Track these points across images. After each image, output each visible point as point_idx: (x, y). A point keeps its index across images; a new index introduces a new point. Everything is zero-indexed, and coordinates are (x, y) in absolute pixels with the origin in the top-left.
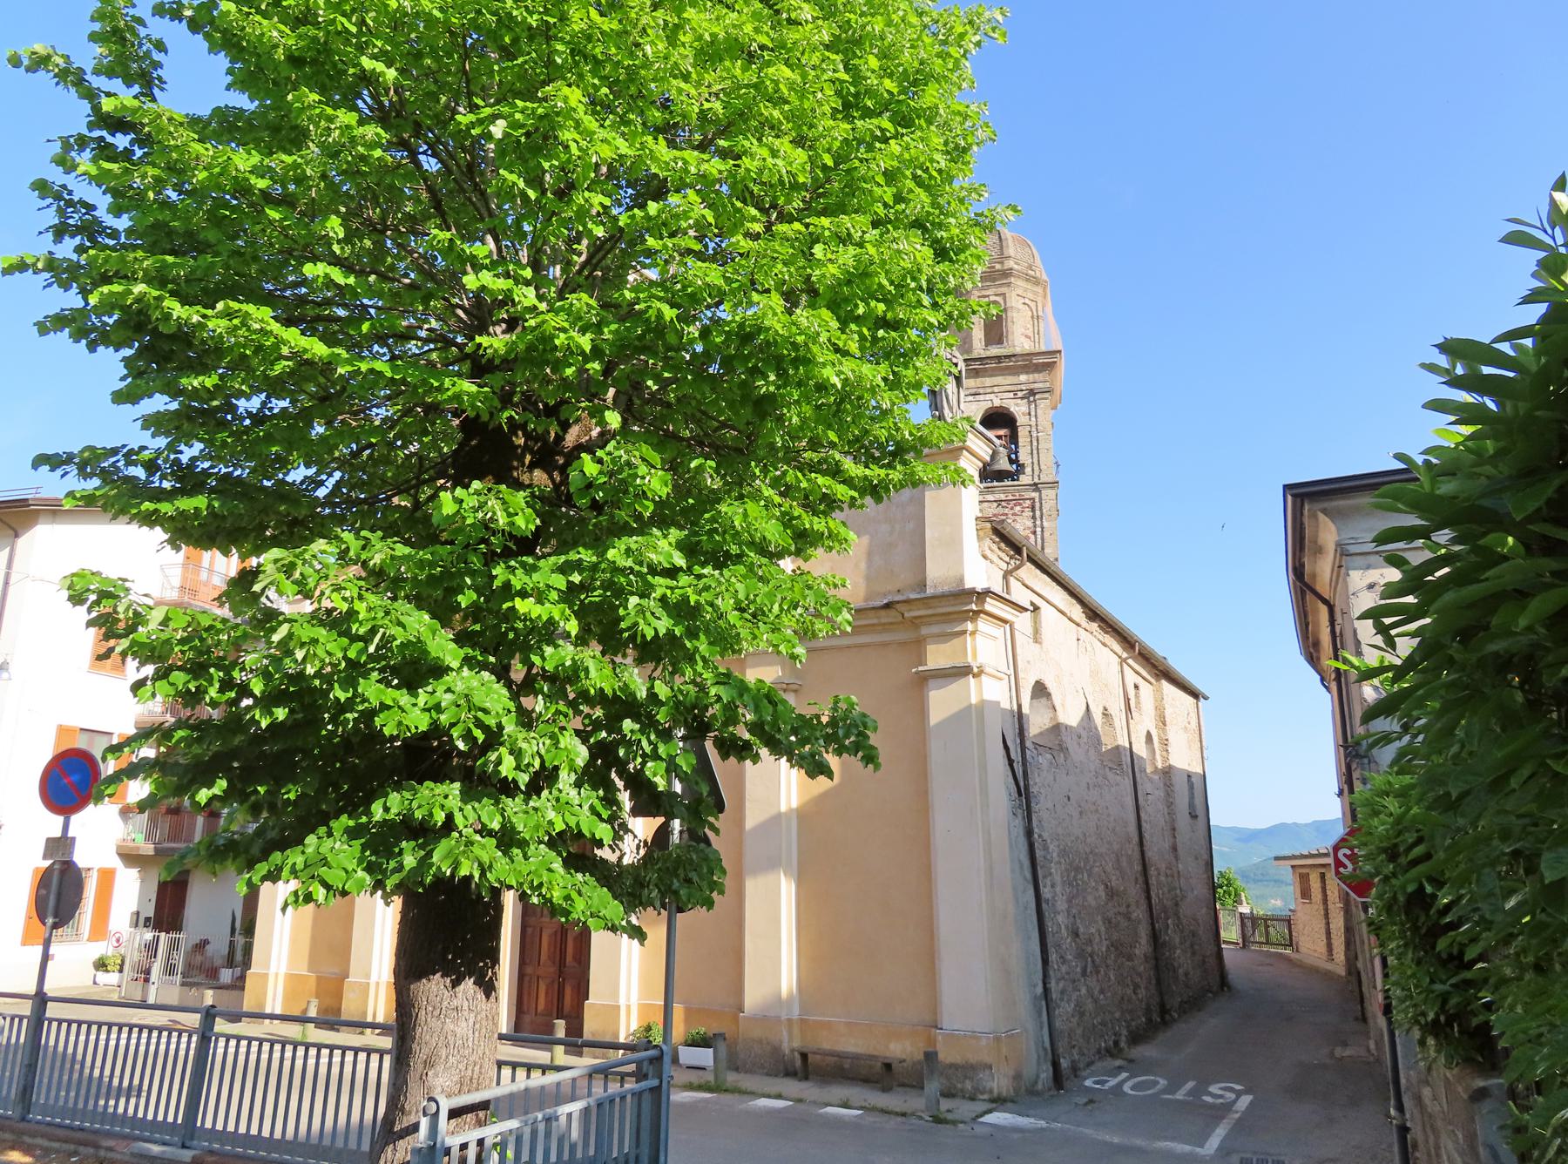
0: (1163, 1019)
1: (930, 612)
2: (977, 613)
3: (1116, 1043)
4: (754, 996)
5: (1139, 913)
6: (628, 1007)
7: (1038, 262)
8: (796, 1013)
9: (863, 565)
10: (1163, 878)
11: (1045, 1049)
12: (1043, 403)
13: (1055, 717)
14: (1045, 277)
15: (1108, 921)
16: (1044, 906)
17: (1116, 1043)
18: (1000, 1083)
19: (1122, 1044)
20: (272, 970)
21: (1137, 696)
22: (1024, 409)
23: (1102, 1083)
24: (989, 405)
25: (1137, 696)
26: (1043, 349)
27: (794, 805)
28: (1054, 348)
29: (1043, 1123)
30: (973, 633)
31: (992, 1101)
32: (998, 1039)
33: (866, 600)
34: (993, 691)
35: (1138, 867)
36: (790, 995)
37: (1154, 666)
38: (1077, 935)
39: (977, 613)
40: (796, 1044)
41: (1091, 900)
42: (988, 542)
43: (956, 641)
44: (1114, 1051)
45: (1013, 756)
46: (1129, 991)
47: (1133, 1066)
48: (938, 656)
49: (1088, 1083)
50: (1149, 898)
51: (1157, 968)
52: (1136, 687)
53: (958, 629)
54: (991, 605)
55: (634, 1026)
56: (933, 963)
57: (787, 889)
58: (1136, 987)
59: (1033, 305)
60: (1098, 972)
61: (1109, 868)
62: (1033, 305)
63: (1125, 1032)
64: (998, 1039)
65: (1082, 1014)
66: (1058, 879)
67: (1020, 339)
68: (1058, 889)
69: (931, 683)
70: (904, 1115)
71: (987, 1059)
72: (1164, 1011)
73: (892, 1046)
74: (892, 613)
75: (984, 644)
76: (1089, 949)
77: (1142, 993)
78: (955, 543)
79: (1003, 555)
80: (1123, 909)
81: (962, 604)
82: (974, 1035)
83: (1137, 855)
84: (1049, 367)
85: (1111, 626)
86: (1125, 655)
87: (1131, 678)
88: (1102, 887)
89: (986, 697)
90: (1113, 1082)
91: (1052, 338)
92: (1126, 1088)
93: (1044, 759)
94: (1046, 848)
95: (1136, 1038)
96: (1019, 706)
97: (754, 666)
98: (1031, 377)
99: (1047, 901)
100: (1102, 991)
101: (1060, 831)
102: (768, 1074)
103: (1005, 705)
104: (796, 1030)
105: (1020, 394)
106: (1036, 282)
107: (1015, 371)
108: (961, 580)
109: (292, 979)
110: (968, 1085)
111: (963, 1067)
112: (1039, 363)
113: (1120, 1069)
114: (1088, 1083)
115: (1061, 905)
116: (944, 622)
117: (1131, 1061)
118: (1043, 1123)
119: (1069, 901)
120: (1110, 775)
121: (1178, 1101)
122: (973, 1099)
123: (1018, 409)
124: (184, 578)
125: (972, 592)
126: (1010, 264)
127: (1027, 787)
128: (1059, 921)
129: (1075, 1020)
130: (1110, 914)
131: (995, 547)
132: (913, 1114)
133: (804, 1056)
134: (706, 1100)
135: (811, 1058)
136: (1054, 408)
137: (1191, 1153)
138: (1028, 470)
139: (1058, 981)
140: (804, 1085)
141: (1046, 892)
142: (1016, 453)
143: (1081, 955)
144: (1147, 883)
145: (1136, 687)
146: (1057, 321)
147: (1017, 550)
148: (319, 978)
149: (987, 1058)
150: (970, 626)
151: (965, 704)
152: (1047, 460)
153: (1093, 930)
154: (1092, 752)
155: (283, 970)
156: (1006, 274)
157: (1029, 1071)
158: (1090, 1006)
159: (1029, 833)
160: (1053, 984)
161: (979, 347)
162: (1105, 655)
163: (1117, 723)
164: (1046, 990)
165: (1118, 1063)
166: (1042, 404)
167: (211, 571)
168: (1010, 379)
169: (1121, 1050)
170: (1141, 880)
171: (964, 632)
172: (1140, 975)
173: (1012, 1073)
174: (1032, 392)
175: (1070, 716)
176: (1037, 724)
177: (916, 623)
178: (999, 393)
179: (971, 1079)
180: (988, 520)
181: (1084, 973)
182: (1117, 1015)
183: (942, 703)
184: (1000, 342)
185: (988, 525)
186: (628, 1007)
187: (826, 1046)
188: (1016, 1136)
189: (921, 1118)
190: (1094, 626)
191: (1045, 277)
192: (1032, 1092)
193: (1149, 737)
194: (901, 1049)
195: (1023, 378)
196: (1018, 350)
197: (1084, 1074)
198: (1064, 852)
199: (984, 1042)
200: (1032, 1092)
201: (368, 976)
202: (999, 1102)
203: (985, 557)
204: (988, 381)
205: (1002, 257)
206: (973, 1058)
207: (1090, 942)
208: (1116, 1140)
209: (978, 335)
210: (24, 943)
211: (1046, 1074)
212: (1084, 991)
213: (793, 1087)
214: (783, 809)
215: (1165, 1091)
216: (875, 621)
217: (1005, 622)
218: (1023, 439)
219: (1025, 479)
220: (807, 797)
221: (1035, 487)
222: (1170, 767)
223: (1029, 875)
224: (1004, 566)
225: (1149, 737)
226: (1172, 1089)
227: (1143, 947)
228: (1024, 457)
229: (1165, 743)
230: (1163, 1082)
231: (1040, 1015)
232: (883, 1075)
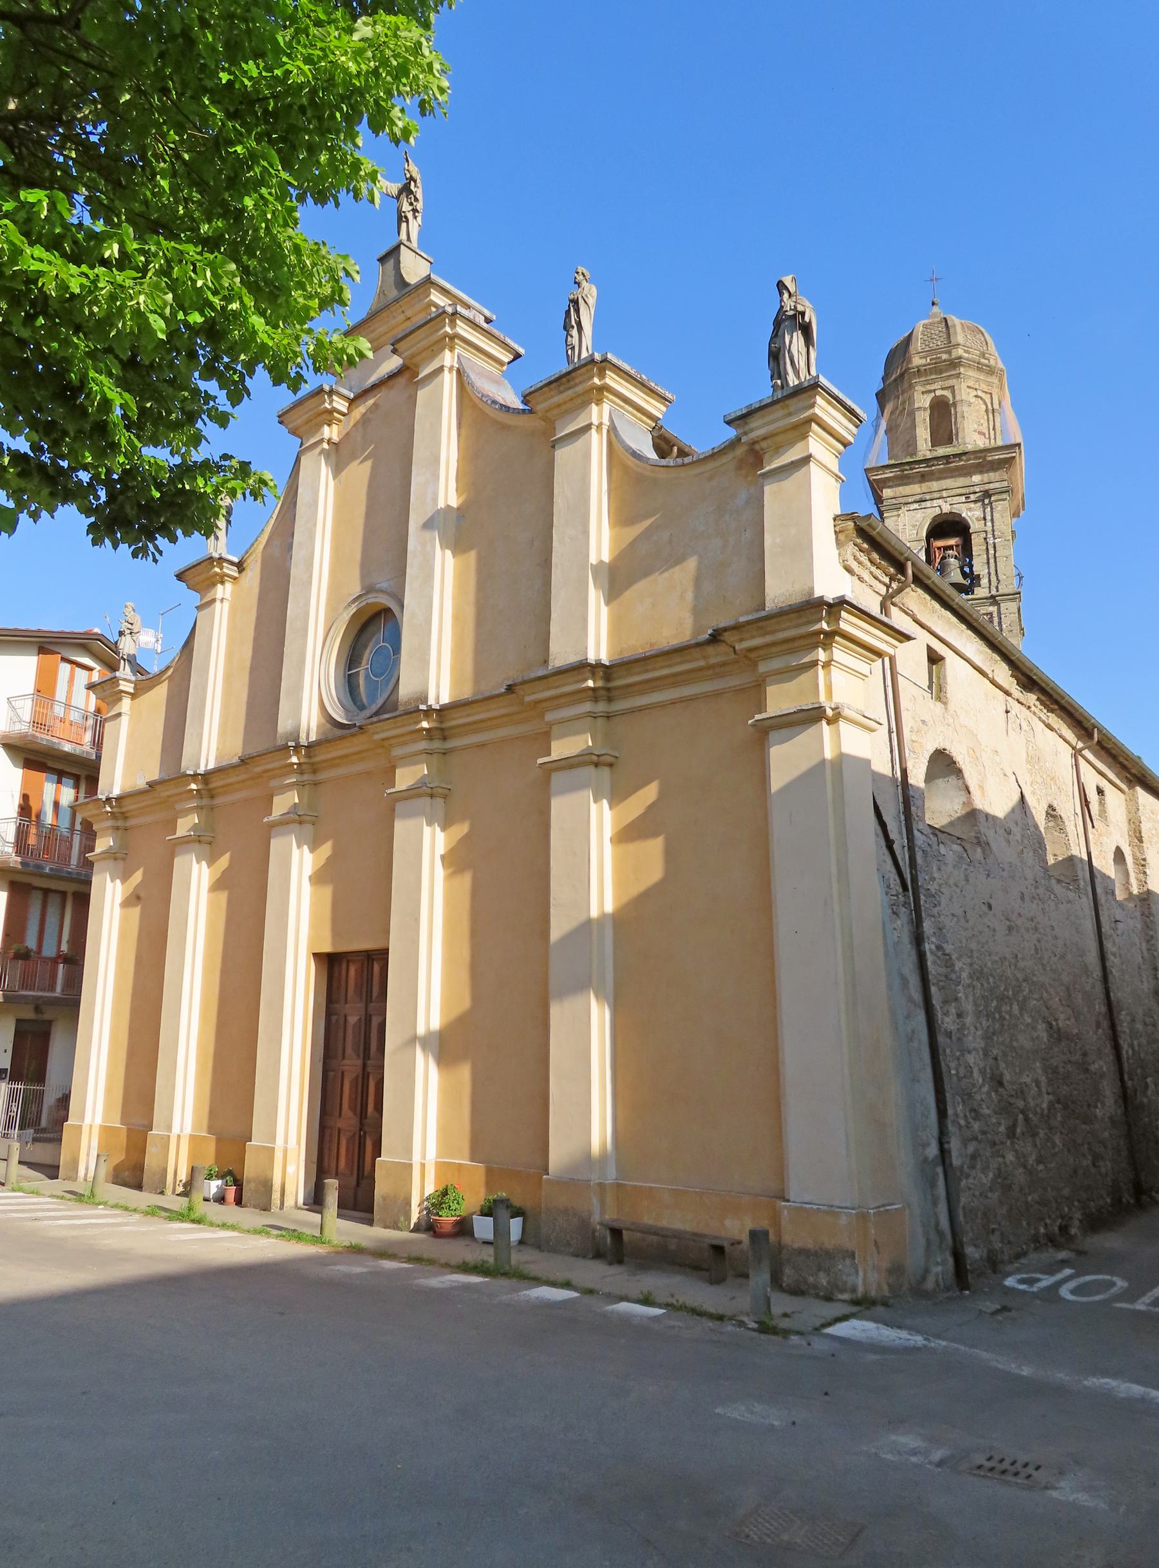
0: (1138, 1200)
1: (768, 639)
2: (830, 635)
3: (1064, 1229)
4: (559, 1154)
5: (1103, 1064)
6: (423, 1165)
7: (992, 348)
8: (611, 1175)
9: (690, 595)
10: (1139, 1026)
11: (940, 1233)
12: (1002, 508)
13: (969, 802)
14: (1001, 365)
15: (1053, 1072)
16: (941, 1039)
17: (1064, 1229)
18: (866, 1277)
19: (1073, 1231)
20: (416, 1159)
21: (1102, 803)
22: (979, 513)
23: (1031, 1282)
24: (938, 511)
25: (1102, 803)
26: (1000, 443)
27: (609, 908)
28: (1013, 442)
29: (918, 1340)
30: (827, 665)
31: (856, 1302)
32: (863, 1217)
34: (868, 747)
35: (1100, 1007)
36: (604, 1156)
37: (1124, 767)
38: (1001, 1084)
39: (830, 635)
40: (610, 1216)
41: (1023, 1040)
42: (851, 549)
43: (804, 678)
44: (1060, 1238)
45: (893, 835)
46: (1087, 1162)
47: (1083, 1260)
48: (780, 699)
49: (1010, 1282)
50: (1117, 1048)
51: (1129, 1135)
52: (1100, 791)
53: (807, 659)
54: (848, 623)
55: (430, 1189)
57: (599, 1017)
58: (1097, 1158)
59: (987, 398)
60: (1034, 1135)
61: (1055, 1002)
62: (987, 398)
63: (1078, 1215)
64: (863, 1217)
65: (1007, 1188)
66: (969, 1007)
67: (973, 433)
68: (969, 1020)
69: (773, 735)
70: (720, 1318)
71: (849, 1245)
72: (1139, 1190)
73: (728, 1223)
74: (722, 648)
75: (845, 680)
76: (1021, 1104)
77: (1106, 1166)
78: (803, 549)
79: (878, 573)
80: (1077, 1057)
81: (812, 622)
82: (832, 1211)
83: (1099, 988)
84: (1008, 463)
85: (1056, 702)
86: (1080, 745)
87: (1092, 781)
88: (1042, 1026)
89: (846, 749)
90: (1046, 1281)
92: (1065, 1292)
93: (949, 852)
94: (949, 963)
95: (1095, 1223)
96: (904, 772)
97: (562, 736)
98: (986, 477)
99: (949, 1035)
100: (1039, 1161)
101: (973, 946)
102: (576, 1255)
103: (882, 765)
104: (609, 1199)
105: (973, 497)
106: (991, 371)
107: (967, 471)
108: (812, 589)
109: (106, 1130)
110: (823, 1279)
111: (816, 1254)
112: (995, 460)
113: (1064, 1263)
114: (1010, 1282)
115: (974, 1040)
116: (792, 651)
117: (1080, 1253)
118: (918, 1340)
119: (988, 1037)
120: (1058, 889)
121: (1139, 1313)
122: (829, 1298)
123: (971, 514)
124: (35, 713)
125: (821, 603)
127: (914, 879)
128: (970, 1061)
129: (995, 1196)
130: (1054, 1062)
131: (864, 558)
132: (731, 1318)
133: (616, 1233)
134: (467, 1287)
135: (626, 1235)
136: (1016, 514)
137: (1143, 1399)
138: (984, 582)
139: (965, 1142)
140: (615, 1269)
141: (947, 1022)
142: (971, 566)
143: (1005, 1108)
144: (1113, 1026)
145: (1100, 791)
146: (1015, 411)
147: (901, 568)
148: (128, 1129)
149: (847, 1242)
150: (822, 655)
151: (815, 761)
152: (1006, 569)
153: (1028, 1080)
154: (1029, 856)
155: (98, 1121)
156: (955, 364)
157: (914, 1260)
158: (1020, 1176)
159: (918, 939)
160: (954, 1145)
161: (923, 445)
162: (1054, 744)
163: (1070, 827)
164: (944, 1153)
165: (1063, 1255)
166: (999, 507)
167: (68, 705)
168: (961, 481)
169: (1071, 1238)
170: (1105, 1024)
171: (815, 663)
172: (1102, 1143)
173: (885, 1264)
174: (987, 494)
175: (996, 802)
176: (941, 809)
177: (751, 658)
178: (950, 496)
179: (827, 1271)
180: (851, 517)
181: (1011, 1133)
182: (1066, 1192)
183: (786, 761)
184: (949, 441)
185: (851, 524)
186: (423, 1165)
187: (648, 1220)
188: (872, 1357)
189: (741, 1324)
190: (1032, 698)
191: (1001, 365)
192: (918, 1292)
193: (1119, 855)
194: (735, 1228)
195: (976, 478)
196: (970, 448)
197: (1009, 1268)
198: (978, 974)
199: (843, 1221)
200: (918, 1292)
202: (864, 1305)
203: (849, 570)
204: (935, 485)
205: (950, 345)
206: (829, 1243)
207: (1021, 1093)
208: (1026, 1371)
209: (923, 434)
211: (942, 1267)
212: (1010, 1157)
213: (594, 1273)
214: (594, 913)
215: (1119, 1297)
216: (702, 663)
217: (879, 654)
218: (977, 542)
219: (981, 592)
220: (625, 899)
221: (993, 600)
222: (1149, 892)
223: (917, 996)
224: (883, 590)
225: (1119, 855)
226: (1131, 1295)
227: (1108, 1106)
228: (979, 567)
229: (1142, 864)
230: (1121, 1284)
231: (933, 1185)
232: (713, 1260)
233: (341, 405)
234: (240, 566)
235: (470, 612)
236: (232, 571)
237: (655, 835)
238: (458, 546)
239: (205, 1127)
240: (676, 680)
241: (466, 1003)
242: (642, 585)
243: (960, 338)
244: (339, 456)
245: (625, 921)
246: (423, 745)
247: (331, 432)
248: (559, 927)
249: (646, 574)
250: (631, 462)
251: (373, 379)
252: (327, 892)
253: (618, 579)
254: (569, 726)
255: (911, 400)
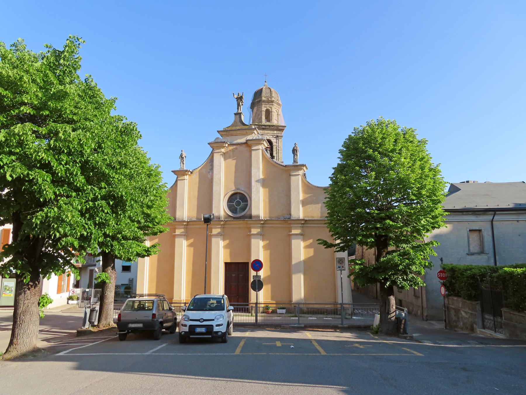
7: (279, 99)
9: (320, 210)
22: (275, 141)
27: (302, 258)
33: (321, 217)
56: (335, 291)
84: (282, 130)
91: (282, 123)
112: (280, 129)
123: (274, 140)
126: (273, 99)
138: (275, 158)
168: (272, 132)
174: (277, 136)
178: (269, 135)
195: (275, 132)
201: (181, 298)
204: (266, 132)
210: (57, 293)
228: (274, 154)
233: (227, 145)
234: (191, 173)
235: (267, 200)
236: (189, 173)
237: (312, 248)
238: (264, 186)
239: (270, 298)
240: (318, 224)
241: (269, 273)
242: (310, 206)
243: (273, 95)
244: (225, 156)
245: (305, 261)
246: (260, 225)
247: (223, 150)
248: (294, 262)
249: (311, 204)
250: (307, 183)
251: (235, 142)
252: (228, 251)
253: (305, 203)
254: (296, 228)
255: (261, 109)
